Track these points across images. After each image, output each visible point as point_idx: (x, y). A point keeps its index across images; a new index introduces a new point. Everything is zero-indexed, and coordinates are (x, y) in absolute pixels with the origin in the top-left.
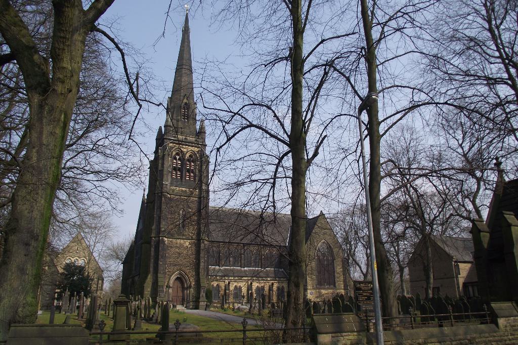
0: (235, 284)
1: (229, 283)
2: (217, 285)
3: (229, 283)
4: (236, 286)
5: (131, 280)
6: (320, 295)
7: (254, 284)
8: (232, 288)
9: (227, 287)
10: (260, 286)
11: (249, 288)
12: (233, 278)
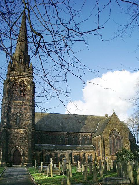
0: (61, 153)
1: (57, 153)
2: (50, 154)
3: (57, 153)
4: (61, 154)
5: (41, 152)
6: (93, 179)
7: (73, 153)
8: (59, 156)
10: (76, 154)
11: (70, 155)
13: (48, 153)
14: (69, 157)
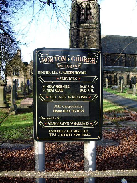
0: (120, 75)
1: (116, 75)
3: (116, 75)
4: (120, 76)
9: (116, 76)
12: (118, 72)
13: (109, 74)
14: (127, 78)
